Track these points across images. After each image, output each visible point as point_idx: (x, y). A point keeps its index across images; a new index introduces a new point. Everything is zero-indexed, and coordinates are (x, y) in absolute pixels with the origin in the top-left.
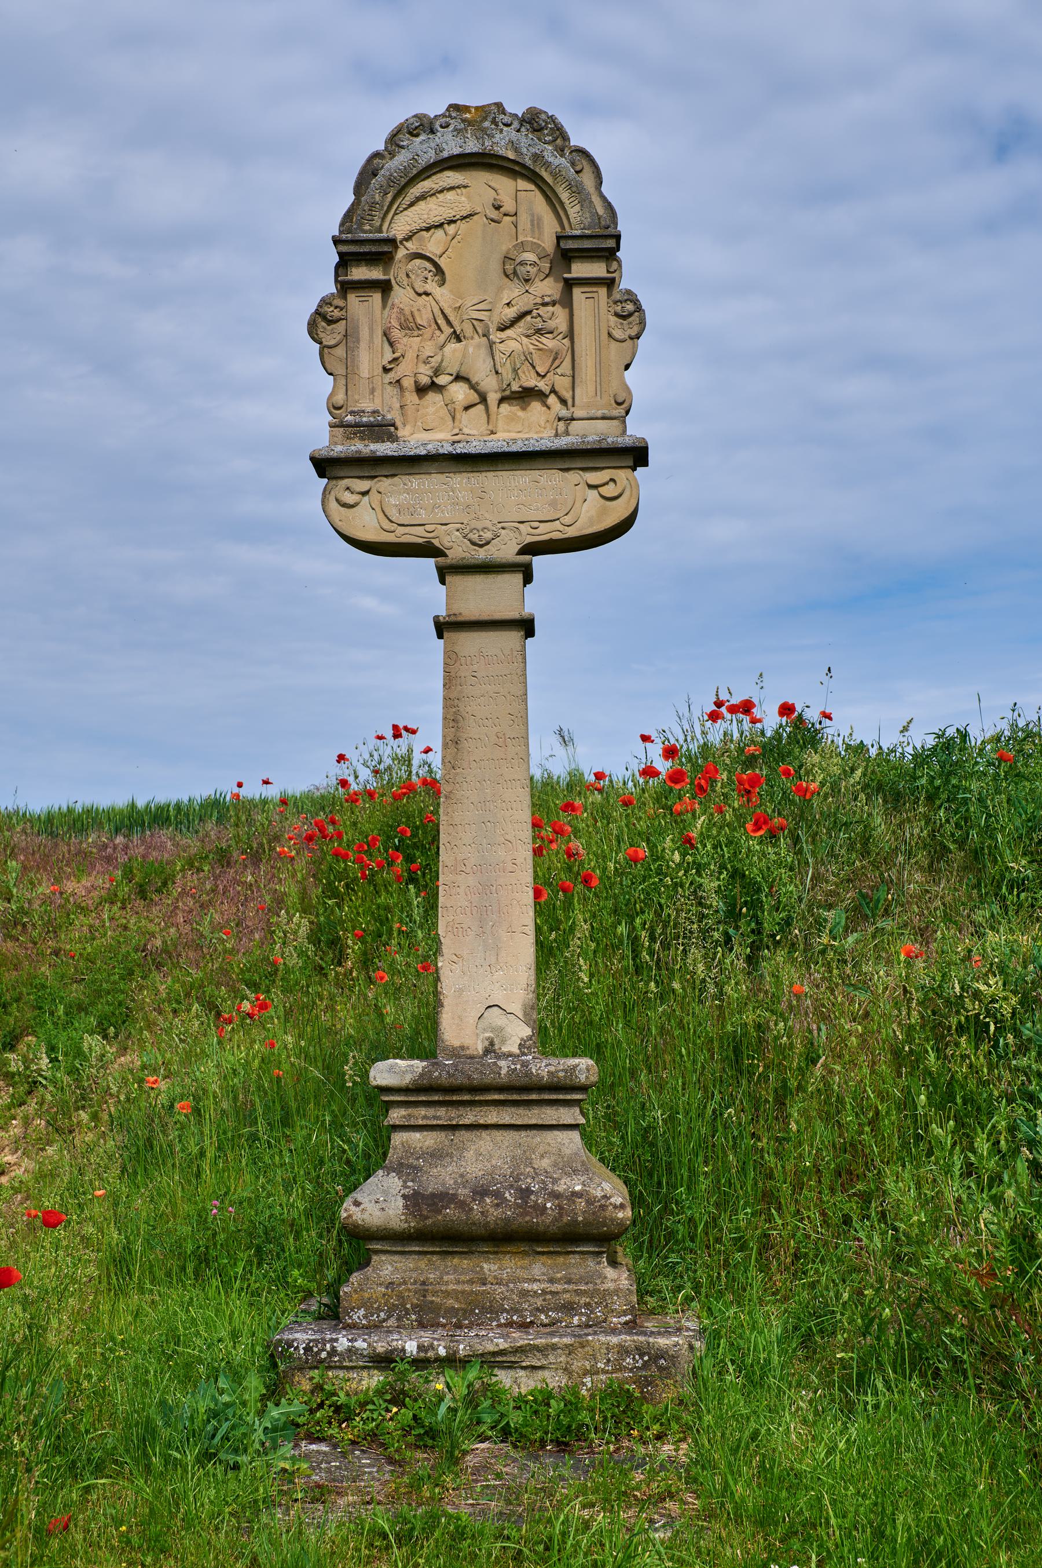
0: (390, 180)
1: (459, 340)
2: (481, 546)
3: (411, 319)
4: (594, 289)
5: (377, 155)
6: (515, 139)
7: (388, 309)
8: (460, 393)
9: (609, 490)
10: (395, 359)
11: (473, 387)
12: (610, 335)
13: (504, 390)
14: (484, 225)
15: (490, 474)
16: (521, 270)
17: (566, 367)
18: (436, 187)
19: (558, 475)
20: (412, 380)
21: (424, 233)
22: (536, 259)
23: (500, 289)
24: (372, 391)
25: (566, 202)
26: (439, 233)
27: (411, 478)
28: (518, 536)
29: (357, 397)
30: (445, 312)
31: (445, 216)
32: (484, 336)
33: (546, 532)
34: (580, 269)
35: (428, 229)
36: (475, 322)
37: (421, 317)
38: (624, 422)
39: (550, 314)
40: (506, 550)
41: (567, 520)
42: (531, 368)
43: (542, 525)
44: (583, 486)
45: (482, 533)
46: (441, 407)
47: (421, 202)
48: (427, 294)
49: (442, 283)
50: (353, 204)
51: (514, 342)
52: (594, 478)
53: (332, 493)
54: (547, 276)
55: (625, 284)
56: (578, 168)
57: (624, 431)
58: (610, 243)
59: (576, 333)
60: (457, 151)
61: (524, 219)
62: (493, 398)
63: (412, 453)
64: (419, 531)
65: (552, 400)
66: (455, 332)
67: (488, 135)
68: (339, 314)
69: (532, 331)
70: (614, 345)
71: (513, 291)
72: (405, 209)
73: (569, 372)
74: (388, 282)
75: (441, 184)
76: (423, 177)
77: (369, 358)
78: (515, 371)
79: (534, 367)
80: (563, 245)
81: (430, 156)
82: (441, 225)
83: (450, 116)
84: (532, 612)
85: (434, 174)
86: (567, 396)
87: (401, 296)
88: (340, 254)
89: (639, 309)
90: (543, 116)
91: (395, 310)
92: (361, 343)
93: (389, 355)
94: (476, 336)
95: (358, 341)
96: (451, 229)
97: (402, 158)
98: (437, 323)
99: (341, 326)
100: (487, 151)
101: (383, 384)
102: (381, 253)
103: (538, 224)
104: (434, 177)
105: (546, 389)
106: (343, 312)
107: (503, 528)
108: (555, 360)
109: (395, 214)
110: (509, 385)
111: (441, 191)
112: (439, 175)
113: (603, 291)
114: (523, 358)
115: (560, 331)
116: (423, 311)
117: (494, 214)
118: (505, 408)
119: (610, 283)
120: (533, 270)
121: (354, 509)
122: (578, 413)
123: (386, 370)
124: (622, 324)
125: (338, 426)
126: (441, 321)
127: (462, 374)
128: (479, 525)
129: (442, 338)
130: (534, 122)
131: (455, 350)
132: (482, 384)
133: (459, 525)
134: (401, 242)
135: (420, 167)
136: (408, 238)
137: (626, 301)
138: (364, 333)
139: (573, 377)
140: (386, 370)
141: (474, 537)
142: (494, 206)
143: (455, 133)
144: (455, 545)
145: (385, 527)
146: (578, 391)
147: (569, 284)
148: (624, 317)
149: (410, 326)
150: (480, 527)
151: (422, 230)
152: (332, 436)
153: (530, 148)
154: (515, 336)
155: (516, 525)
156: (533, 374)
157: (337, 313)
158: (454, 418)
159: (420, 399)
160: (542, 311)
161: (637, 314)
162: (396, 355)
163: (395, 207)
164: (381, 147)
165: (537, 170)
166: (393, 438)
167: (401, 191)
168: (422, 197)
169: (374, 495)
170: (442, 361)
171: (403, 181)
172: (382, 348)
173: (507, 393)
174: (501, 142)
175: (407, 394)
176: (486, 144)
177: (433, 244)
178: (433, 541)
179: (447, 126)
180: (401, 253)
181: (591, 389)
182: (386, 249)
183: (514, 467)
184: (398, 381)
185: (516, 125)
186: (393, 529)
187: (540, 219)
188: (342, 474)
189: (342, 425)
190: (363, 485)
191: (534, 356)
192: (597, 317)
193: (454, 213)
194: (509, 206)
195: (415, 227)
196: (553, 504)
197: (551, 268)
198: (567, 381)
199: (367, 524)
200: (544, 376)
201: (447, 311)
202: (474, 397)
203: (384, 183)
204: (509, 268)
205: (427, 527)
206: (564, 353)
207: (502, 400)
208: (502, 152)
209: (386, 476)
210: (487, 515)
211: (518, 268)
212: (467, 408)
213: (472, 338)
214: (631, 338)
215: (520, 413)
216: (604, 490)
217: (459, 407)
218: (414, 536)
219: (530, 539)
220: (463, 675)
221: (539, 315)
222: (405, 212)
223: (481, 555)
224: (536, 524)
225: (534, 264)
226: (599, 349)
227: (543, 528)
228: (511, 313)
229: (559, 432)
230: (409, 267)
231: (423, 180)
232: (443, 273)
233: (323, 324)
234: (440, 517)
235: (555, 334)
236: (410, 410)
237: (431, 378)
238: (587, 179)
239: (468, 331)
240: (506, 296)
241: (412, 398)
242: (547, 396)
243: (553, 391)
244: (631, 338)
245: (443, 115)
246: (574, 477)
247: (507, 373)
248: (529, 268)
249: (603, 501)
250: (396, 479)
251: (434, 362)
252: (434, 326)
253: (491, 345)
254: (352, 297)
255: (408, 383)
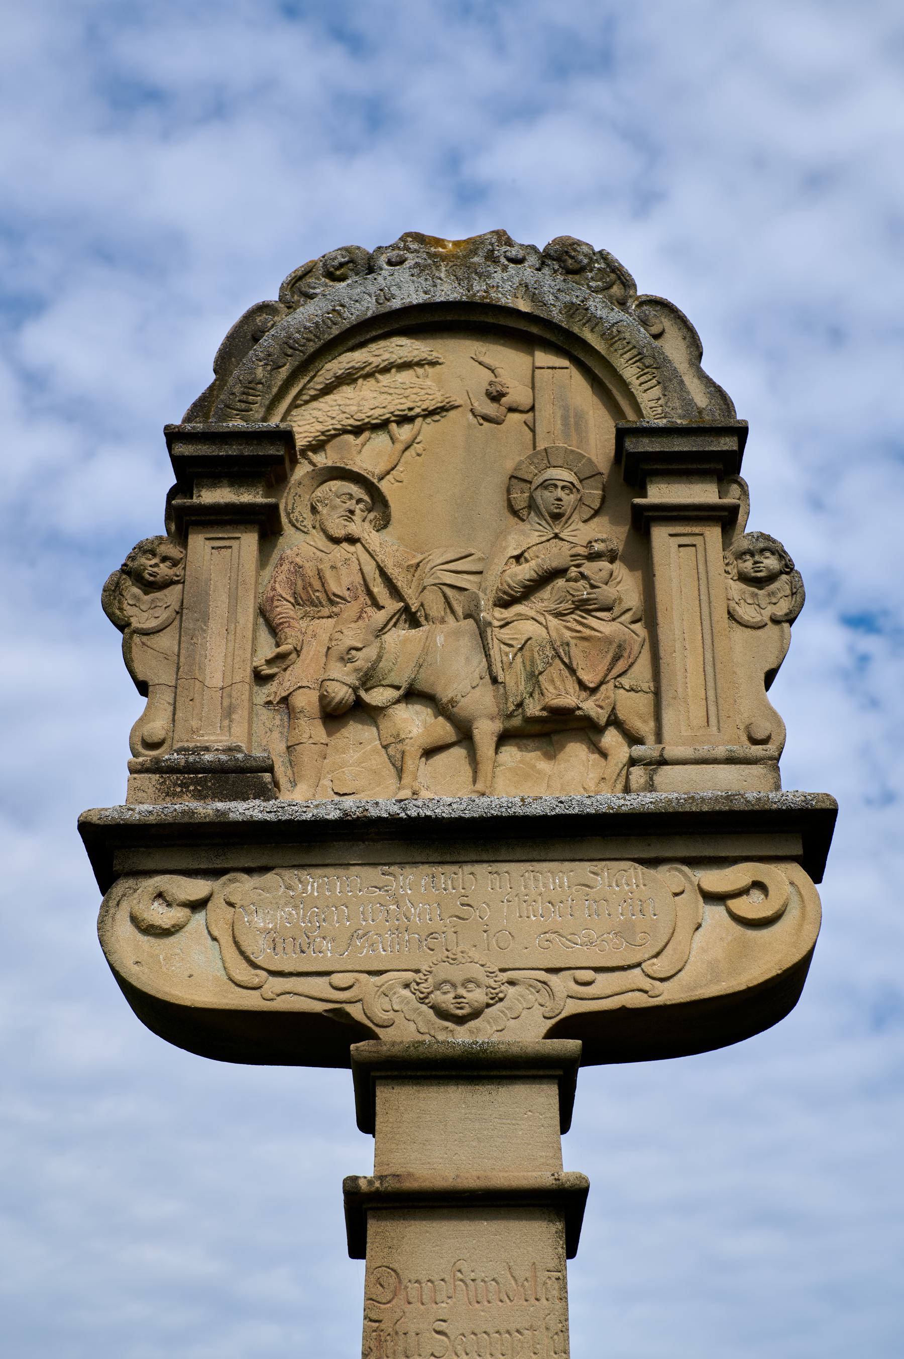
0: (288, 345)
1: (414, 621)
2: (461, 1020)
3: (317, 585)
4: (696, 530)
5: (263, 308)
6: (531, 281)
7: (269, 570)
8: (415, 723)
9: (752, 906)
10: (281, 657)
11: (442, 708)
12: (731, 616)
13: (510, 716)
14: (470, 426)
15: (481, 869)
16: (546, 498)
17: (641, 672)
18: (376, 361)
19: (633, 873)
20: (314, 696)
21: (350, 438)
22: (572, 478)
23: (501, 535)
24: (229, 712)
25: (634, 382)
26: (380, 440)
27: (304, 874)
28: (544, 997)
29: (194, 723)
30: (389, 571)
31: (391, 408)
32: (467, 616)
33: (611, 993)
34: (661, 493)
35: (357, 431)
36: (447, 590)
37: (338, 580)
38: (777, 769)
39: (604, 574)
40: (521, 1026)
41: (659, 967)
42: (566, 673)
43: (601, 977)
44: (692, 897)
45: (461, 991)
46: (374, 751)
47: (345, 388)
48: (352, 540)
49: (384, 523)
50: (211, 388)
51: (531, 624)
52: (716, 879)
53: (125, 905)
54: (597, 513)
55: (757, 521)
56: (655, 330)
57: (778, 787)
58: (728, 444)
59: (660, 607)
60: (417, 298)
61: (547, 416)
62: (486, 731)
63: (308, 816)
64: (319, 986)
65: (611, 739)
66: (407, 609)
67: (480, 275)
68: (171, 572)
69: (569, 605)
70: (740, 634)
71: (528, 535)
72: (314, 398)
73: (647, 684)
74: (273, 509)
75: (386, 356)
76: (351, 343)
77: (226, 651)
78: (533, 677)
79: (573, 671)
80: (632, 445)
81: (368, 307)
82: (382, 426)
83: (407, 249)
84: (585, 1173)
85: (374, 340)
86: (646, 728)
87: (299, 545)
88: (178, 463)
89: (788, 568)
90: (585, 249)
91: (285, 567)
92: (212, 624)
93: (267, 650)
94: (450, 619)
95: (205, 617)
96: (404, 433)
97: (308, 312)
98: (370, 593)
99: (172, 595)
100: (477, 299)
101: (252, 705)
102: (267, 459)
103: (577, 424)
104: (373, 347)
105: (601, 716)
106: (178, 570)
107: (512, 983)
108: (616, 658)
109: (294, 406)
110: (520, 705)
111: (386, 370)
112: (382, 343)
113: (714, 534)
114: (550, 653)
115: (625, 606)
116: (343, 571)
117: (490, 409)
118: (511, 754)
119: (727, 518)
120: (569, 499)
121: (172, 939)
122: (672, 751)
123: (261, 679)
124: (754, 595)
125: (147, 771)
126: (379, 589)
127: (422, 686)
128: (456, 973)
129: (380, 617)
130: (566, 258)
131: (406, 640)
132: (463, 702)
133: (410, 975)
134: (303, 452)
135: (346, 324)
136: (318, 446)
137: (762, 551)
138: (219, 603)
139: (657, 694)
140: (261, 679)
141: (445, 999)
142: (488, 394)
143: (416, 271)
144: (399, 1019)
145: (238, 978)
146: (668, 716)
147: (643, 521)
148: (759, 582)
149: (315, 597)
150: (458, 978)
151: (345, 431)
152: (134, 789)
153: (561, 296)
154: (532, 613)
155: (542, 975)
156: (571, 685)
157: (164, 570)
158: (400, 772)
159: (330, 733)
160: (589, 568)
161: (784, 577)
162: (283, 648)
163: (294, 392)
164: (272, 296)
165: (576, 330)
166: (265, 793)
167: (308, 363)
168: (348, 378)
169: (217, 911)
170: (380, 658)
171: (312, 347)
172: (254, 639)
173: (517, 721)
174: (506, 288)
175: (302, 722)
176: (476, 288)
177: (369, 455)
178: (349, 1008)
179: (401, 262)
180: (302, 470)
181: (697, 713)
182: (272, 451)
183: (534, 855)
184: (285, 700)
185: (532, 260)
186: (256, 981)
187: (580, 417)
188: (149, 865)
189: (156, 768)
190: (197, 888)
191: (574, 651)
192: (702, 578)
193: (410, 404)
194: (518, 394)
195: (330, 425)
196: (625, 932)
197: (603, 499)
198: (644, 702)
199: (197, 974)
200: (593, 691)
201: (391, 570)
202: (444, 730)
203: (275, 350)
204: (520, 498)
205: (337, 979)
206: (636, 648)
207: (504, 738)
208: (507, 301)
209: (249, 871)
210: (474, 954)
211: (538, 495)
212: (429, 752)
213: (443, 621)
214: (776, 621)
215: (544, 765)
216: (740, 906)
217: (413, 750)
218: (304, 997)
219: (573, 1008)
220: (412, 1328)
221: (583, 576)
222: (314, 404)
223: (462, 1037)
224: (588, 975)
225: (570, 487)
226: (710, 641)
227: (604, 983)
228: (525, 572)
229: (634, 785)
230: (319, 493)
231: (352, 349)
232: (385, 504)
233: (136, 590)
234: (366, 957)
235: (617, 611)
236: (307, 754)
237: (355, 689)
238: (674, 348)
239: (435, 606)
240: (513, 544)
241: (312, 730)
242: (600, 730)
243: (614, 721)
244: (776, 621)
245: (394, 247)
246: (670, 877)
247: (515, 681)
248: (560, 493)
249: (738, 929)
250: (270, 877)
251: (363, 659)
252: (364, 598)
253: (482, 629)
254: (198, 542)
255: (307, 700)
